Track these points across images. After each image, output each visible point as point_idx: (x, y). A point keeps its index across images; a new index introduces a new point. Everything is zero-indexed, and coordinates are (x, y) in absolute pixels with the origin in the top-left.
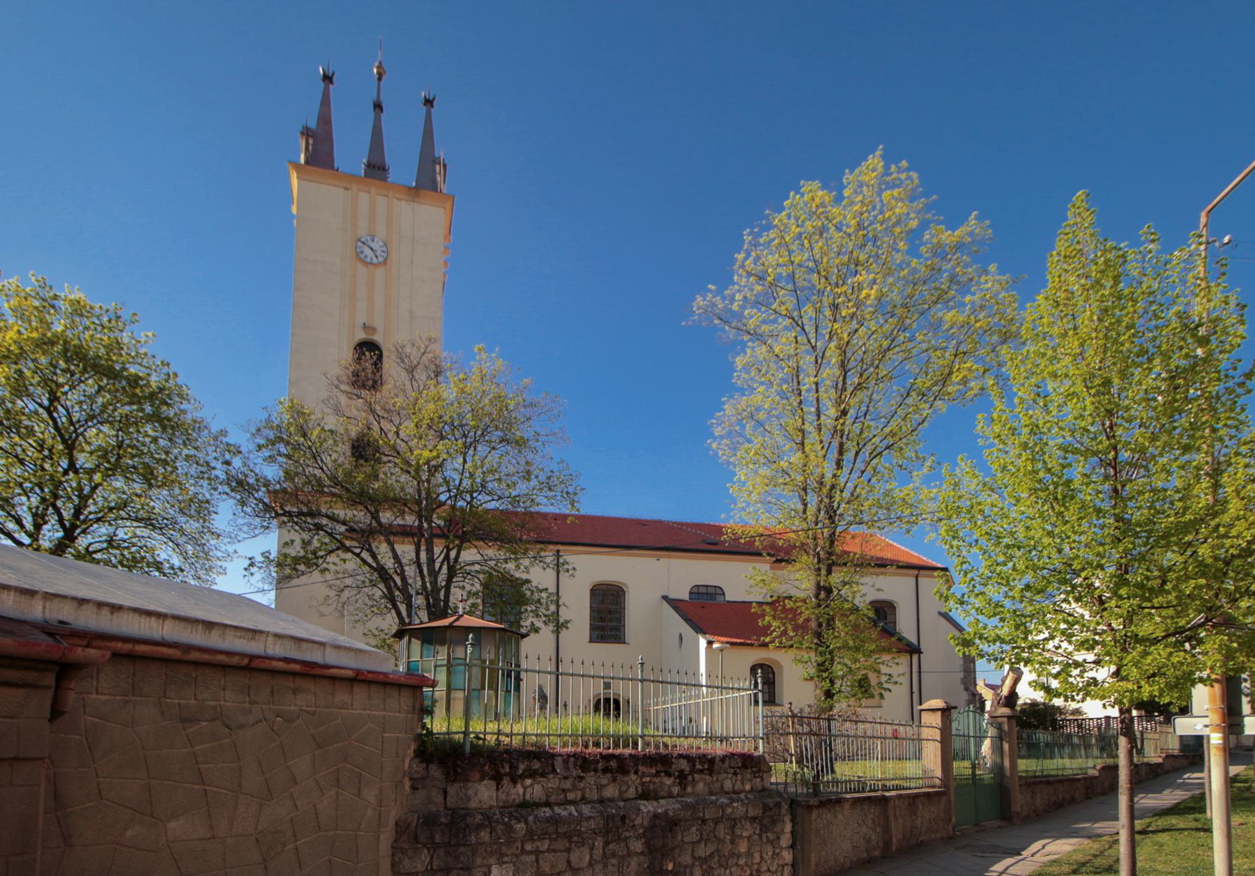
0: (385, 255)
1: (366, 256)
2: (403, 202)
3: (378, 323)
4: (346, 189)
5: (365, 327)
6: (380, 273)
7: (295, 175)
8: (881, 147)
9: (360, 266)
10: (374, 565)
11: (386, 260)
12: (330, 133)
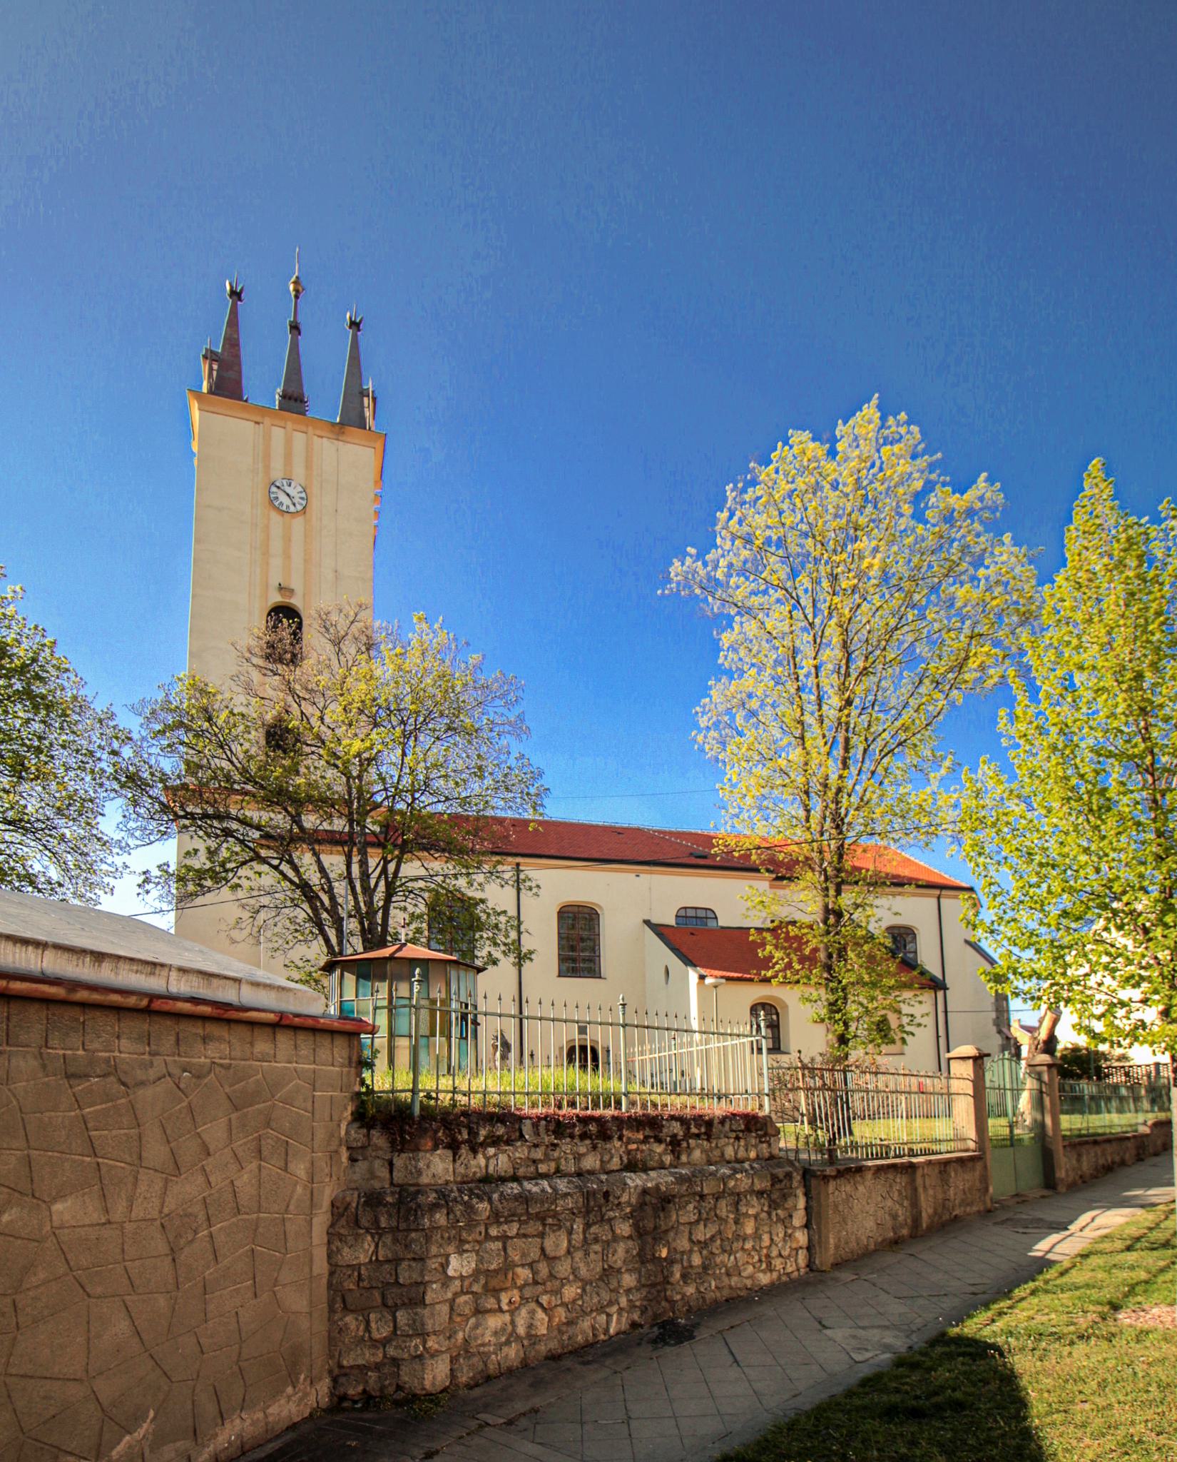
1: (281, 504)
2: (325, 439)
3: (296, 583)
4: (257, 423)
5: (281, 588)
6: (298, 523)
7: (196, 405)
8: (877, 395)
9: (274, 516)
10: (296, 880)
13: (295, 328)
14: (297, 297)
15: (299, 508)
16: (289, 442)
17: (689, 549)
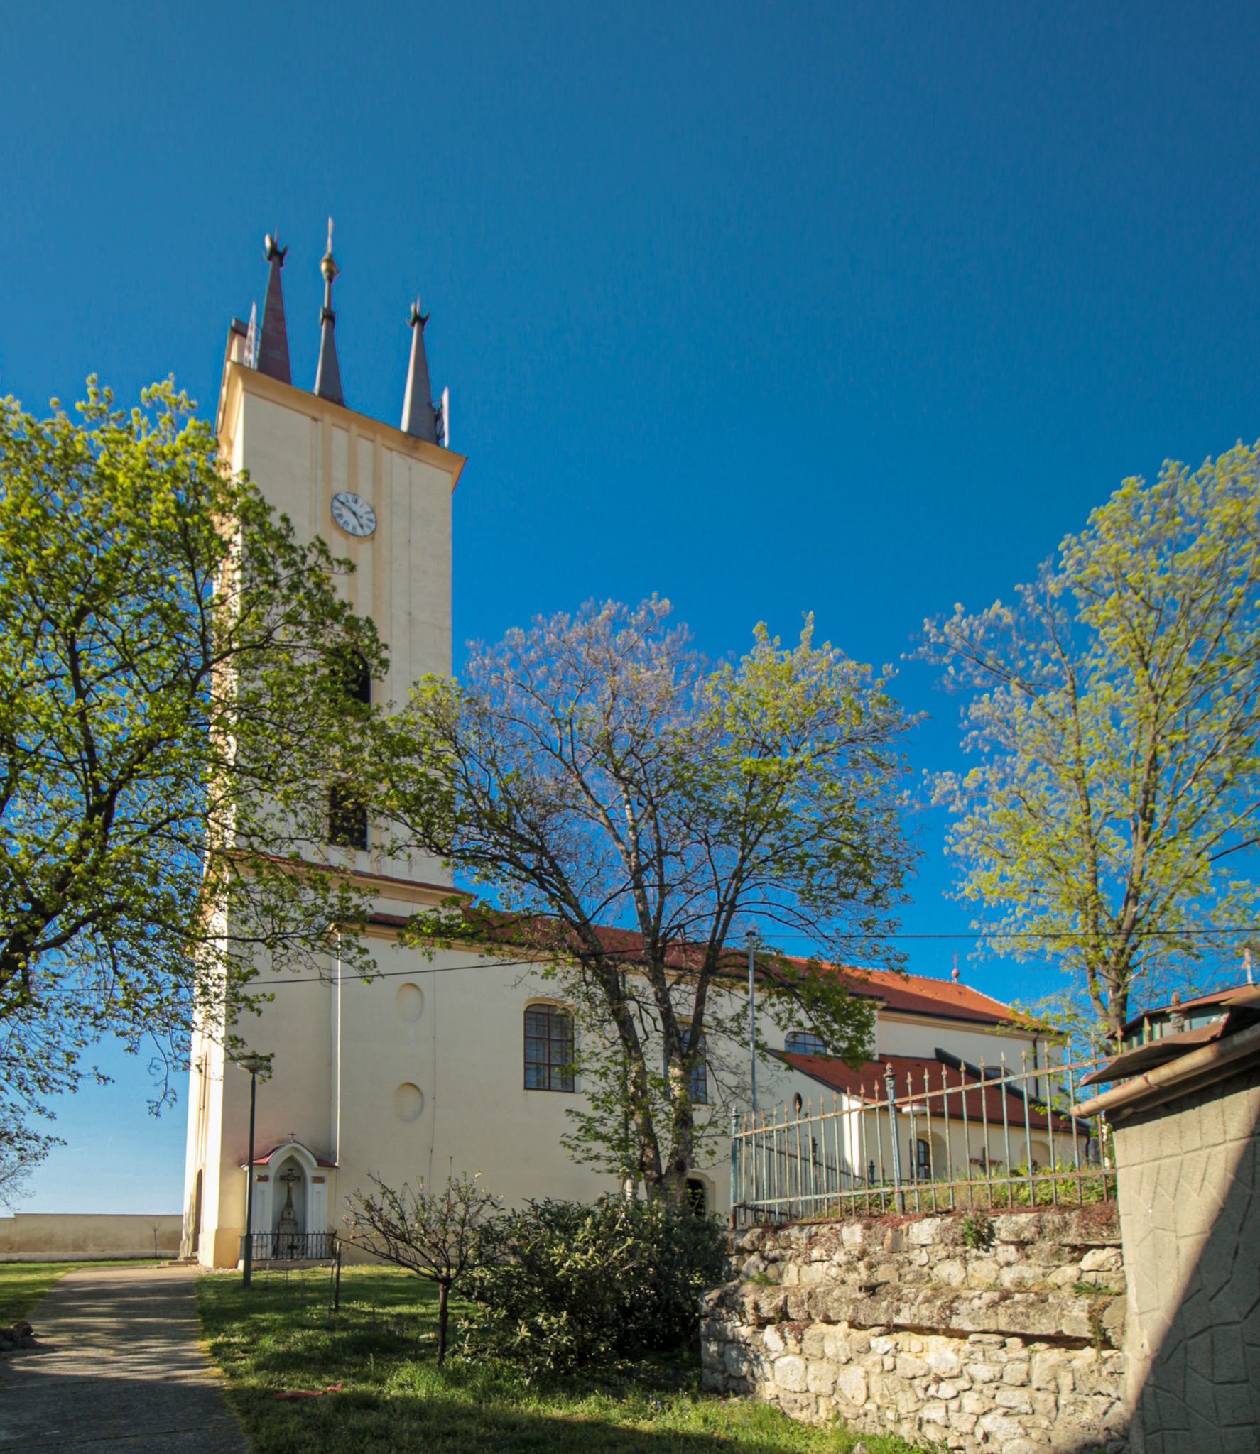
0: (373, 526)
1: (346, 523)
2: (394, 454)
4: (315, 419)
7: (240, 385)
10: (576, 919)
11: (373, 532)
12: (283, 333)
13: (330, 317)
14: (330, 279)
15: (368, 531)
16: (352, 452)
17: (777, 637)
